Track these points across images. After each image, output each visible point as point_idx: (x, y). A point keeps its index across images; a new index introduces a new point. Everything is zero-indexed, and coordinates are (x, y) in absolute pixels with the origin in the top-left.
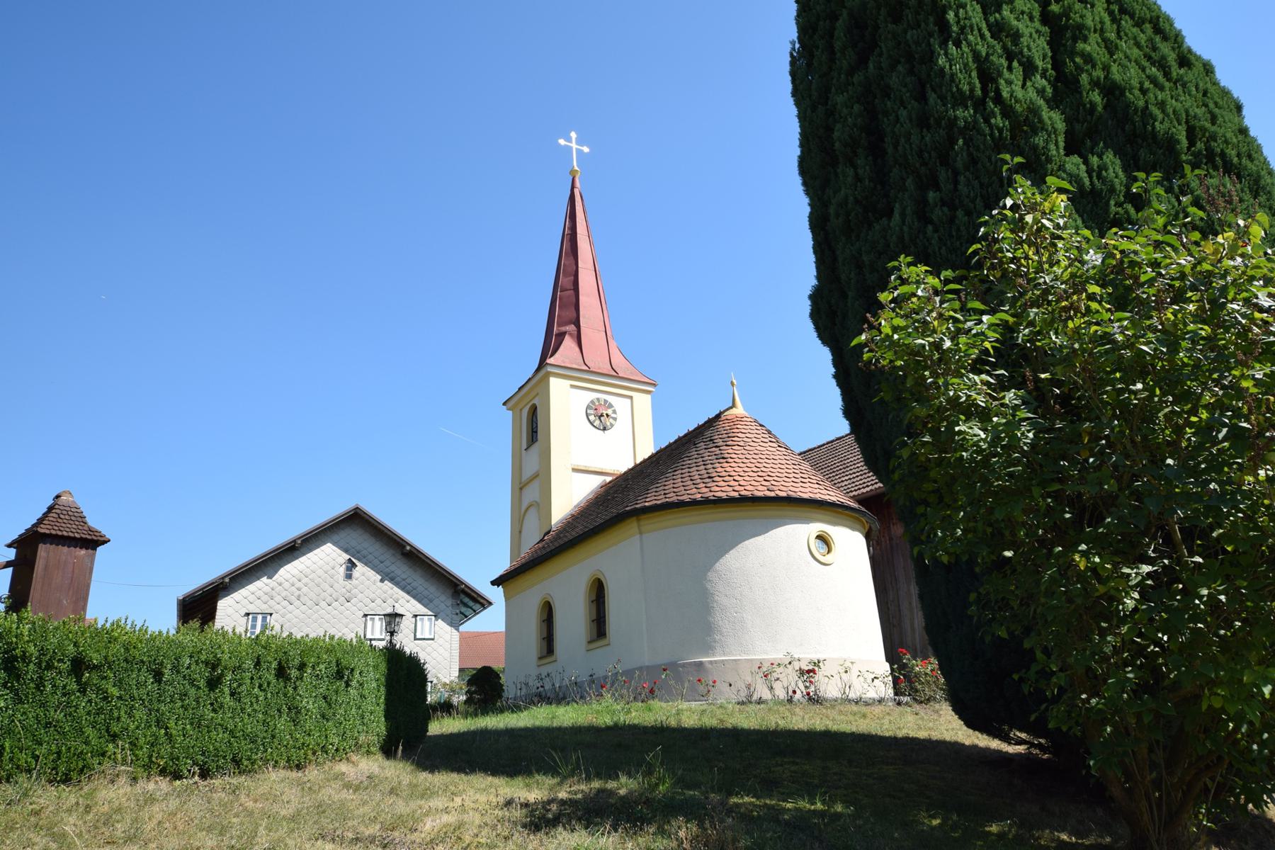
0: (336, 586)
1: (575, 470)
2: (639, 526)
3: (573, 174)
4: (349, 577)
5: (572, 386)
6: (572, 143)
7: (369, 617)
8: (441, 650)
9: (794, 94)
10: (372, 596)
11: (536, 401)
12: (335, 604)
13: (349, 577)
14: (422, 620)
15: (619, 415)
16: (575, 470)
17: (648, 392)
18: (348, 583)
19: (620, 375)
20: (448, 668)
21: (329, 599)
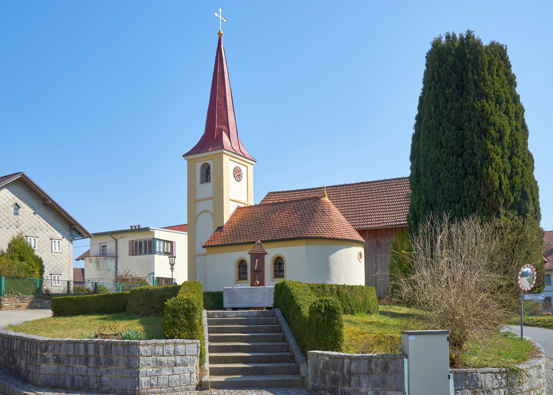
0: (10, 218)
1: (230, 200)
2: (307, 242)
3: (220, 35)
4: (16, 214)
5: (230, 160)
6: (219, 15)
7: (53, 240)
8: (65, 259)
9: (421, 99)
10: (29, 226)
11: (210, 162)
12: (10, 228)
13: (16, 214)
14: (55, 242)
15: (243, 176)
16: (230, 200)
17: (252, 164)
18: (15, 217)
19: (246, 156)
20: (68, 268)
21: (7, 226)
